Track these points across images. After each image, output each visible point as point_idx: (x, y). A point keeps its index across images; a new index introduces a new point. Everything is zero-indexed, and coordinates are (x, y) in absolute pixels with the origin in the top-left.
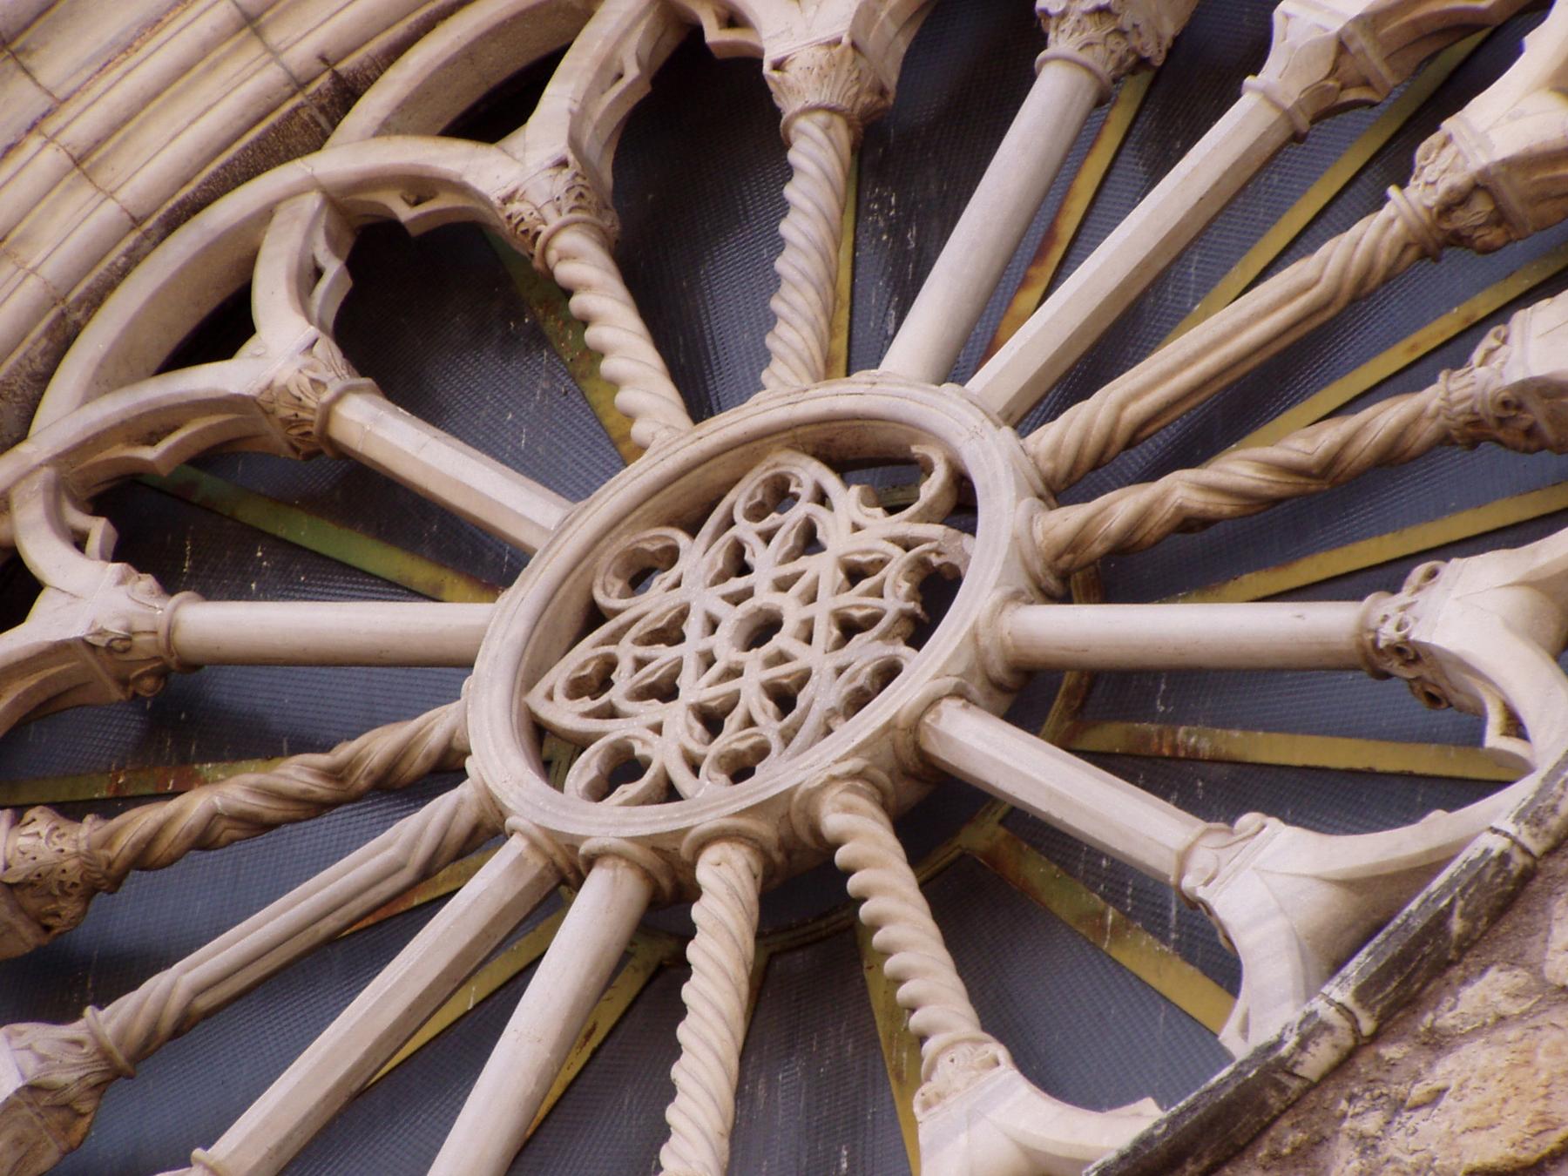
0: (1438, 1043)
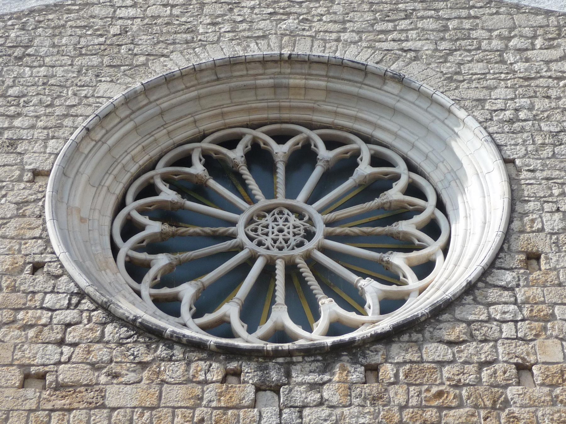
0: (440, 322)
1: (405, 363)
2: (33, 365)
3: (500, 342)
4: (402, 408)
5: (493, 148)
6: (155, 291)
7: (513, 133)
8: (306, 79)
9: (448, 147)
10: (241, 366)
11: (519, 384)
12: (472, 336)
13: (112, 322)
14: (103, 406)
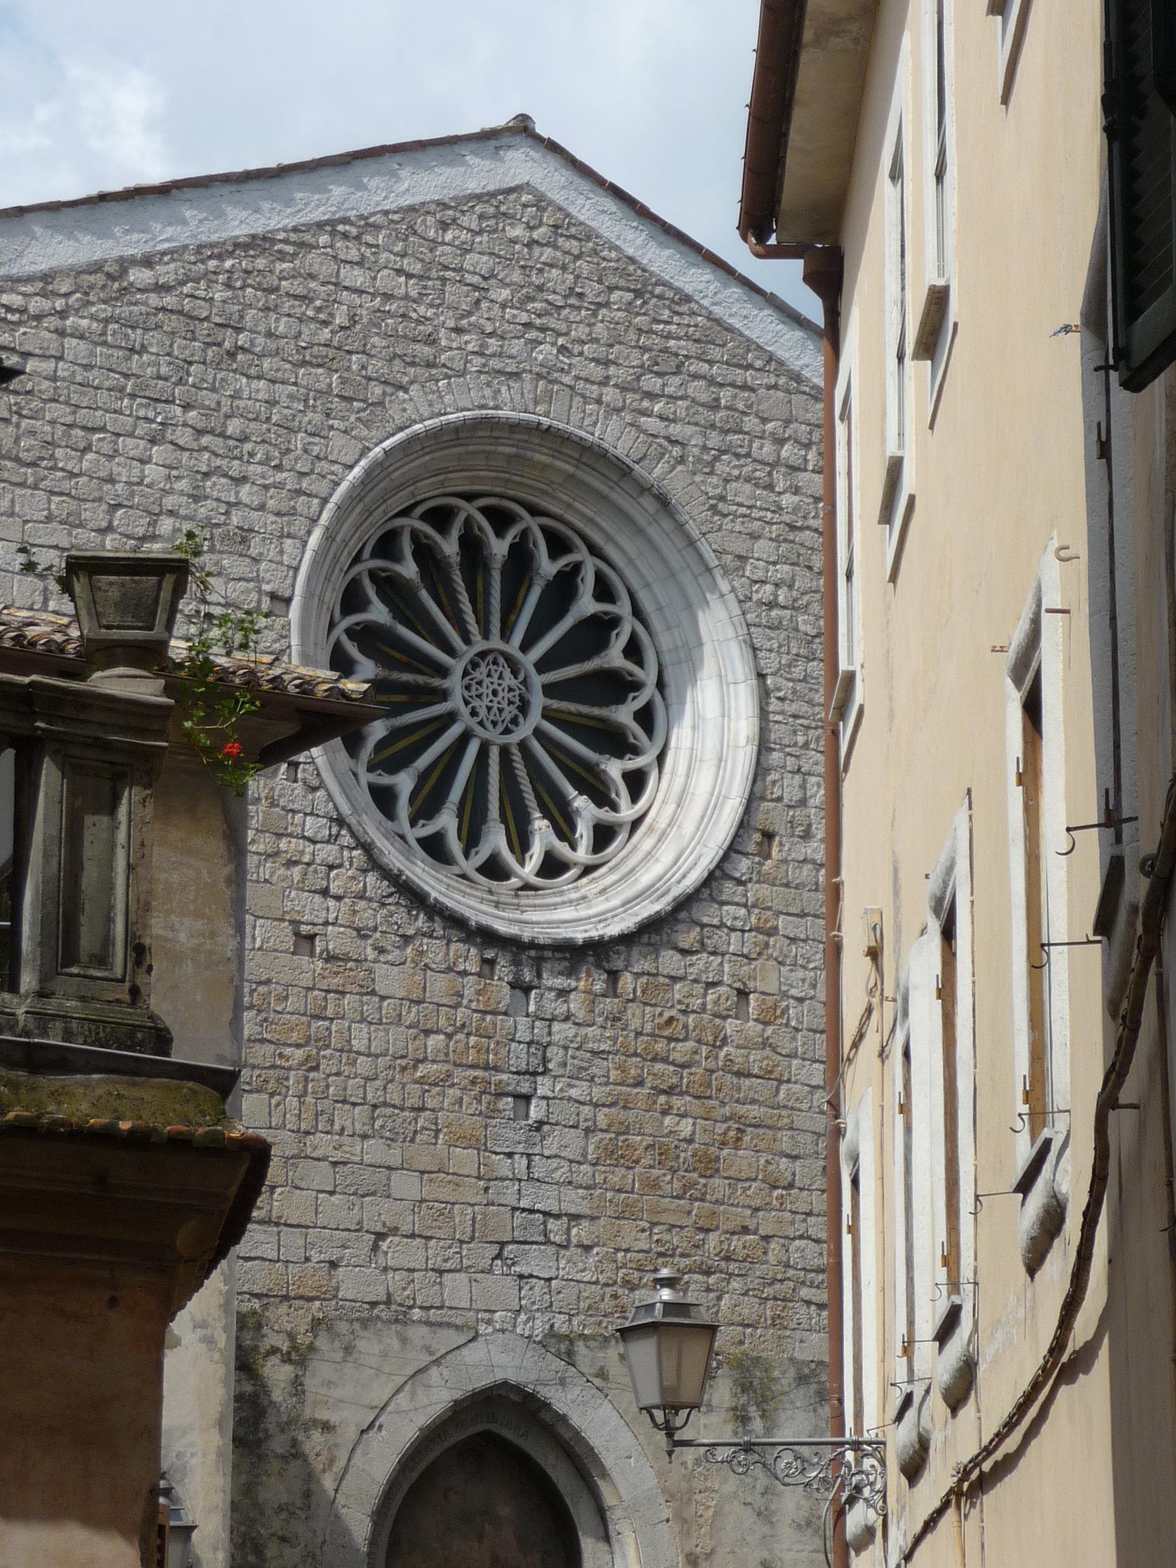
1: (643, 974)
2: (303, 923)
3: (727, 957)
4: (638, 1034)
5: (750, 651)
6: (373, 778)
7: (769, 628)
8: (553, 456)
9: (690, 608)
10: (497, 956)
11: (737, 1018)
12: (702, 944)
13: (372, 870)
14: (373, 993)
